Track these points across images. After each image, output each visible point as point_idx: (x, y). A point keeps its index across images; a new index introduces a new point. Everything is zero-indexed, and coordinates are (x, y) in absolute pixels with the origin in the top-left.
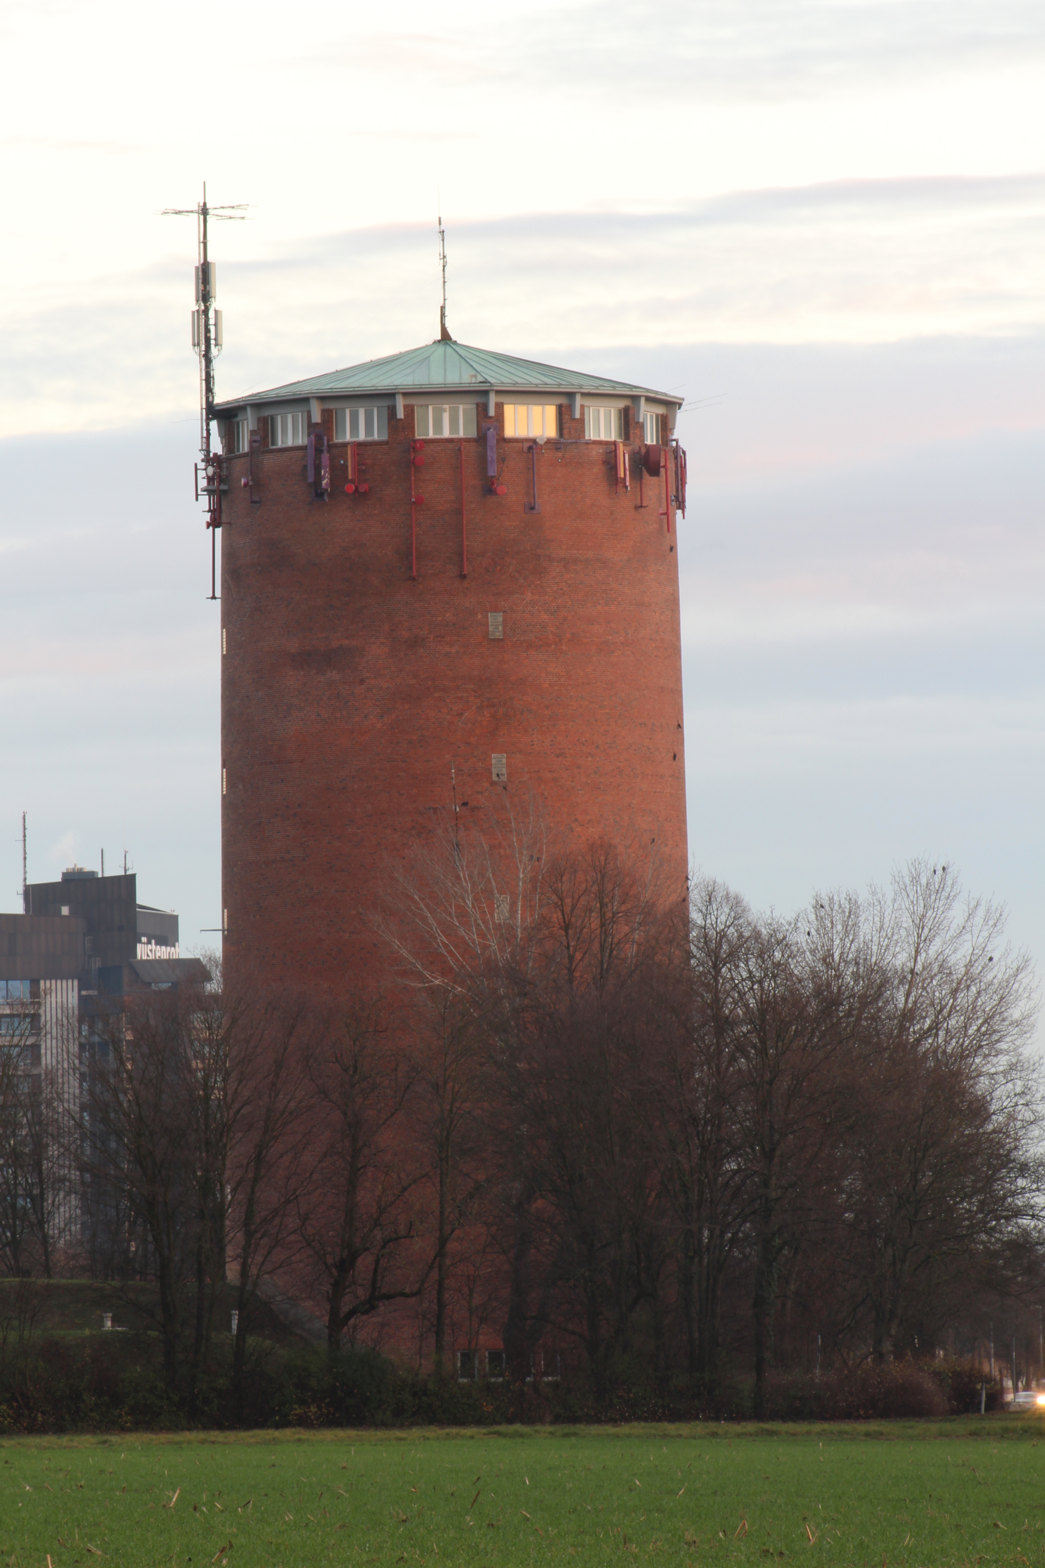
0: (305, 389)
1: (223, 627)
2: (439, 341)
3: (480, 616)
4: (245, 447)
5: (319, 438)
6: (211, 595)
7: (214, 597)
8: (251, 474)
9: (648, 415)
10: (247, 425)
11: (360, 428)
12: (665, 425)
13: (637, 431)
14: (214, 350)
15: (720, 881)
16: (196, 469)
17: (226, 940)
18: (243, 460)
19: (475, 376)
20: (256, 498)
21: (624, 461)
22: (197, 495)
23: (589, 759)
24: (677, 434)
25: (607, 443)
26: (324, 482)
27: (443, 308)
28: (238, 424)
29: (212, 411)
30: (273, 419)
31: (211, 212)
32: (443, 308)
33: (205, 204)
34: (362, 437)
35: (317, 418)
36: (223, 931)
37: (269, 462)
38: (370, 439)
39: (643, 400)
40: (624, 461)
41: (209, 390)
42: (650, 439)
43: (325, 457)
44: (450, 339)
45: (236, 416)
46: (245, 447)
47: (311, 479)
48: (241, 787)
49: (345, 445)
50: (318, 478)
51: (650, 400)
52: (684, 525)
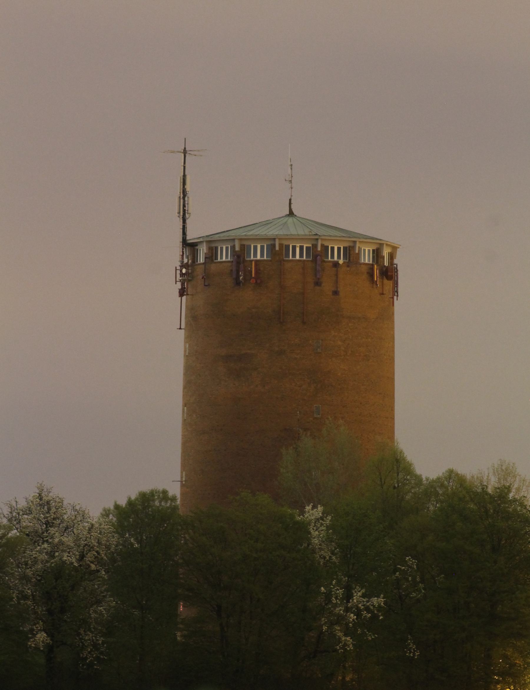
0: (232, 234)
1: (185, 342)
2: (289, 215)
3: (311, 342)
4: (201, 259)
5: (239, 257)
6: (179, 327)
7: (180, 329)
8: (205, 273)
9: (386, 252)
10: (203, 251)
11: (258, 254)
12: (392, 256)
13: (382, 260)
14: (187, 216)
15: (454, 469)
16: (176, 270)
17: (182, 486)
18: (201, 266)
19: (310, 232)
20: (206, 284)
21: (376, 272)
22: (176, 281)
23: (357, 409)
24: (395, 261)
25: (369, 264)
26: (241, 278)
27: (290, 200)
28: (197, 250)
29: (185, 243)
30: (216, 248)
31: (188, 152)
32: (290, 200)
33: (185, 148)
34: (259, 257)
35: (237, 248)
36: (181, 482)
37: (213, 268)
38: (227, 260)
39: (385, 245)
40: (376, 272)
41: (184, 233)
42: (386, 264)
43: (242, 266)
44: (293, 214)
45: (197, 245)
46: (201, 259)
47: (234, 276)
48: (194, 416)
49: (252, 261)
50: (238, 276)
51: (387, 245)
52: (399, 305)
